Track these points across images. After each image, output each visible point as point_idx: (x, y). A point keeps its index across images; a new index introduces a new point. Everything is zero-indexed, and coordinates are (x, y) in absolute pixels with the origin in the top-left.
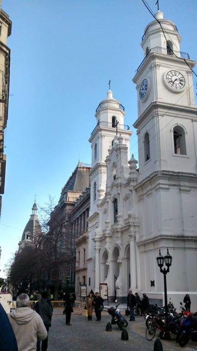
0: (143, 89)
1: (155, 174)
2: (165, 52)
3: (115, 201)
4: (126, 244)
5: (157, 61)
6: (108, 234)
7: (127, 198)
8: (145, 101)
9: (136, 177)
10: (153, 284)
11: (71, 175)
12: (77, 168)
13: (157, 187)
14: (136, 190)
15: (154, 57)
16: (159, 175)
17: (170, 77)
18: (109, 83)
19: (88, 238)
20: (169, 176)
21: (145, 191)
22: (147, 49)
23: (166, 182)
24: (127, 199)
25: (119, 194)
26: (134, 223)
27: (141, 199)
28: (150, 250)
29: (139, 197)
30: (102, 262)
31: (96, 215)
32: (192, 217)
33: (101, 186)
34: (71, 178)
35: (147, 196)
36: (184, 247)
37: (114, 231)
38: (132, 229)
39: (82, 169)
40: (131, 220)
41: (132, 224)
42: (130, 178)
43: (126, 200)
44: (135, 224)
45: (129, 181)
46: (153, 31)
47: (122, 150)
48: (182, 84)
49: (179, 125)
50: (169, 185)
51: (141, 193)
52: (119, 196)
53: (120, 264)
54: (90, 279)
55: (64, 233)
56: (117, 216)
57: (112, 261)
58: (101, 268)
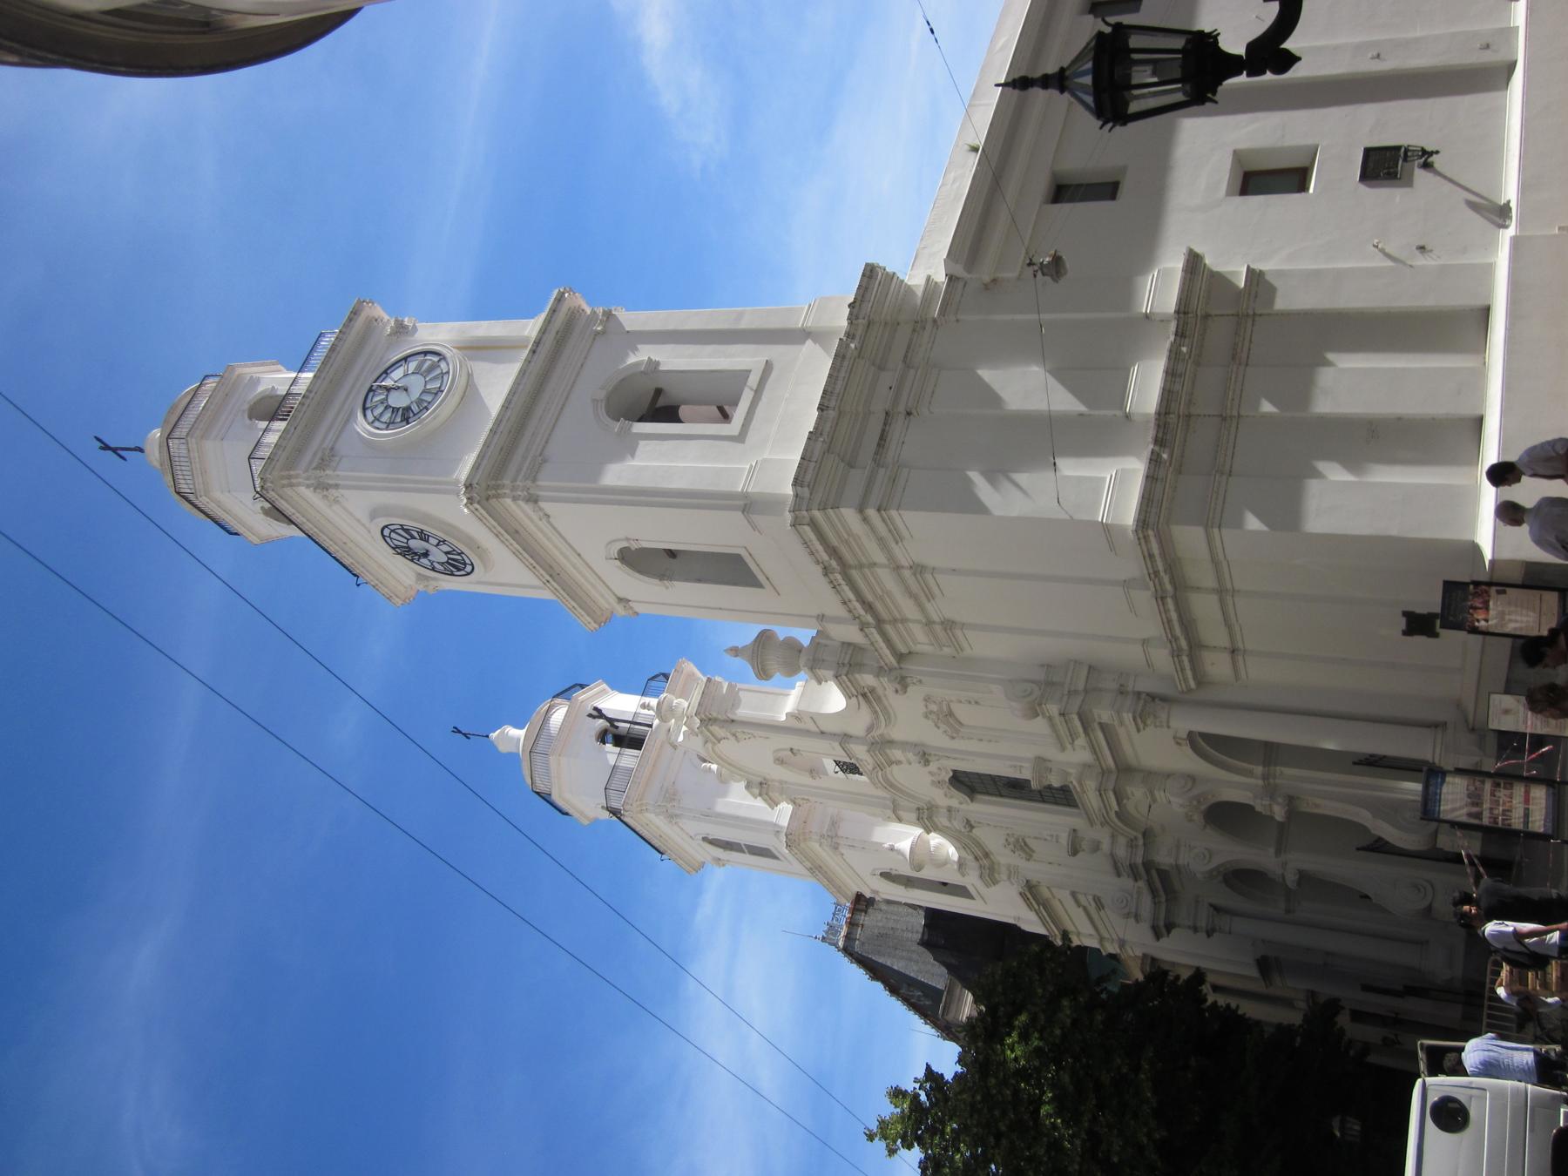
4: (1188, 750)
11: (879, 986)
12: (847, 951)
19: (1154, 960)
21: (909, 609)
24: (951, 714)
28: (1215, 562)
33: (898, 846)
34: (893, 990)
54: (886, 875)
56: (1034, 785)
57: (1278, 852)
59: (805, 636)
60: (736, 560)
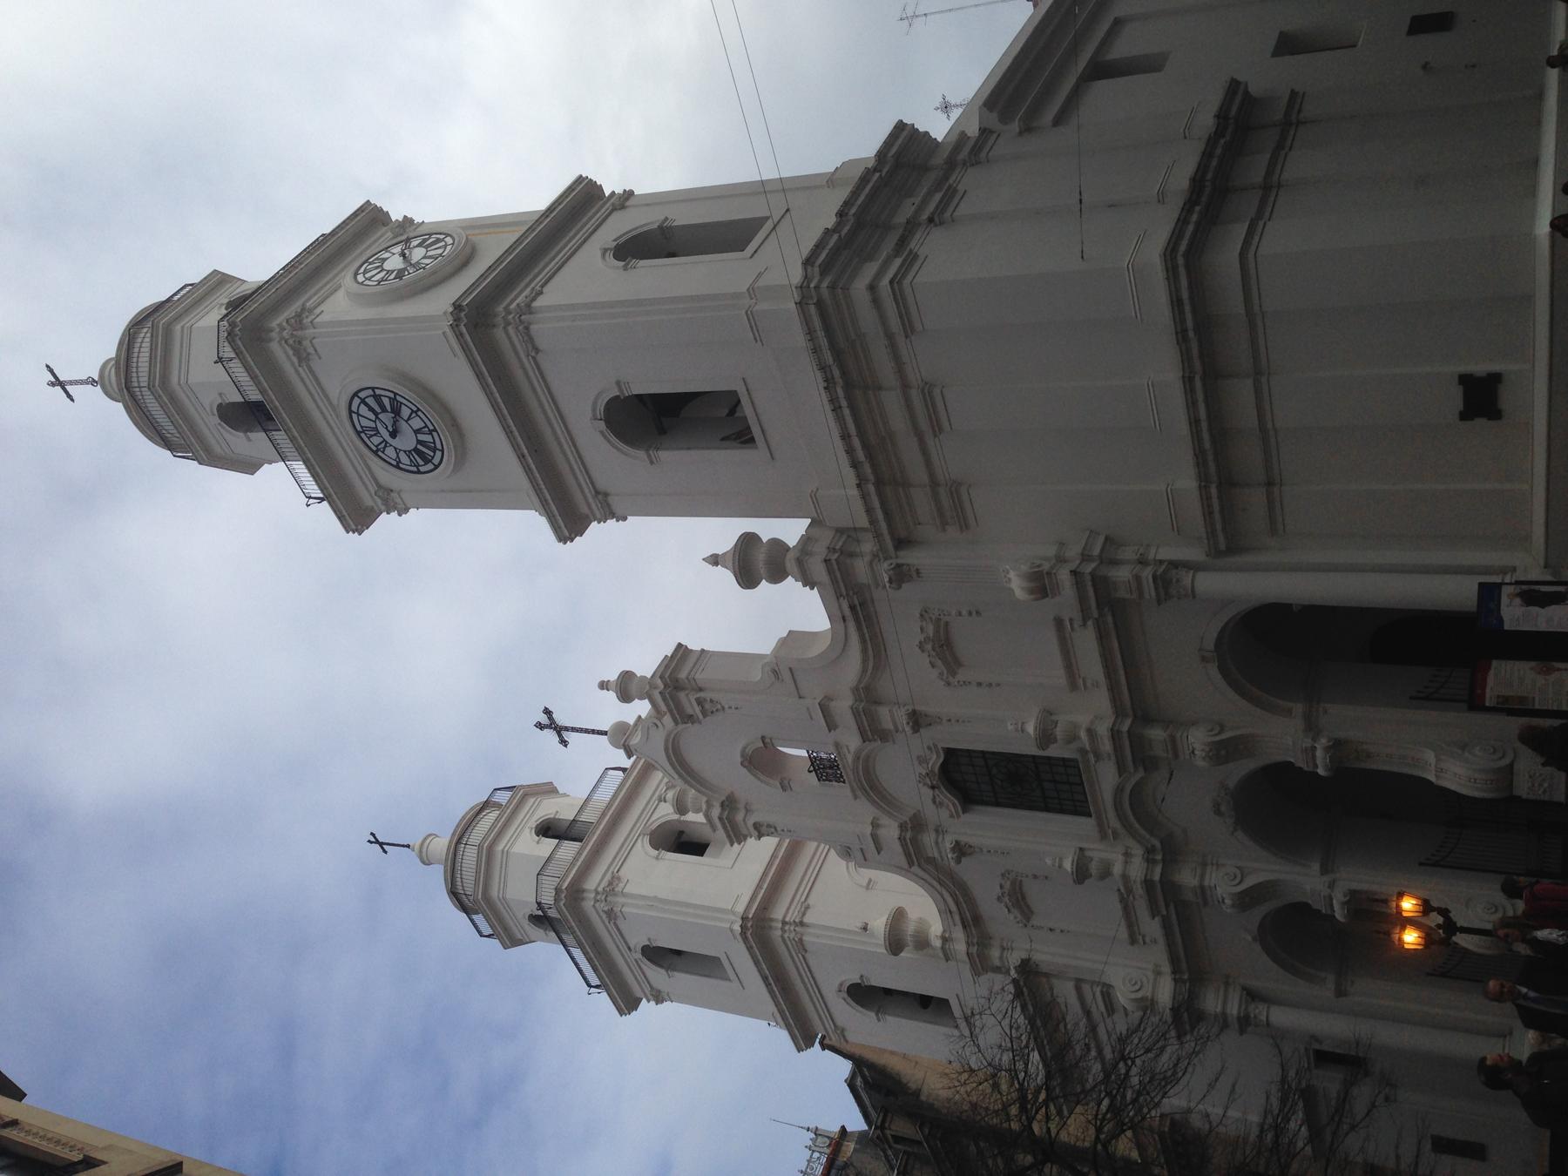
1: (812, 309)
2: (569, 849)
5: (594, 882)
6: (1149, 860)
9: (831, 534)
10: (1481, 397)
14: (901, 543)
15: (574, 894)
16: (825, 284)
22: (534, 919)
37: (1139, 812)
44: (1096, 551)
47: (683, 675)
57: (1325, 870)
59: (791, 530)
60: (714, 961)
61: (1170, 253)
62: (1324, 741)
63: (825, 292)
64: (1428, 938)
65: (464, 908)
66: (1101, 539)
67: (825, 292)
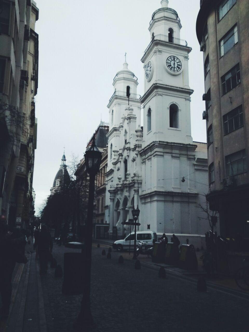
0: (148, 70)
1: (153, 144)
3: (126, 162)
7: (134, 160)
8: (150, 81)
13: (155, 154)
17: (169, 62)
18: (125, 55)
20: (164, 146)
23: (161, 150)
25: (128, 156)
26: (138, 180)
27: (144, 162)
29: (143, 160)
30: (115, 209)
31: (112, 171)
32: (177, 178)
35: (154, 156)
36: (172, 200)
38: (136, 185)
39: (103, 128)
40: (135, 178)
41: (137, 181)
42: (136, 145)
43: (133, 162)
45: (136, 146)
46: (158, 19)
48: (179, 68)
49: (174, 103)
50: (164, 153)
51: (144, 157)
52: (128, 158)
53: (128, 211)
55: (88, 198)
58: (115, 214)
61: (155, 192)
62: (128, 209)
63: (156, 145)
64: (41, 219)
65: (153, 18)
66: (141, 182)
67: (156, 145)
